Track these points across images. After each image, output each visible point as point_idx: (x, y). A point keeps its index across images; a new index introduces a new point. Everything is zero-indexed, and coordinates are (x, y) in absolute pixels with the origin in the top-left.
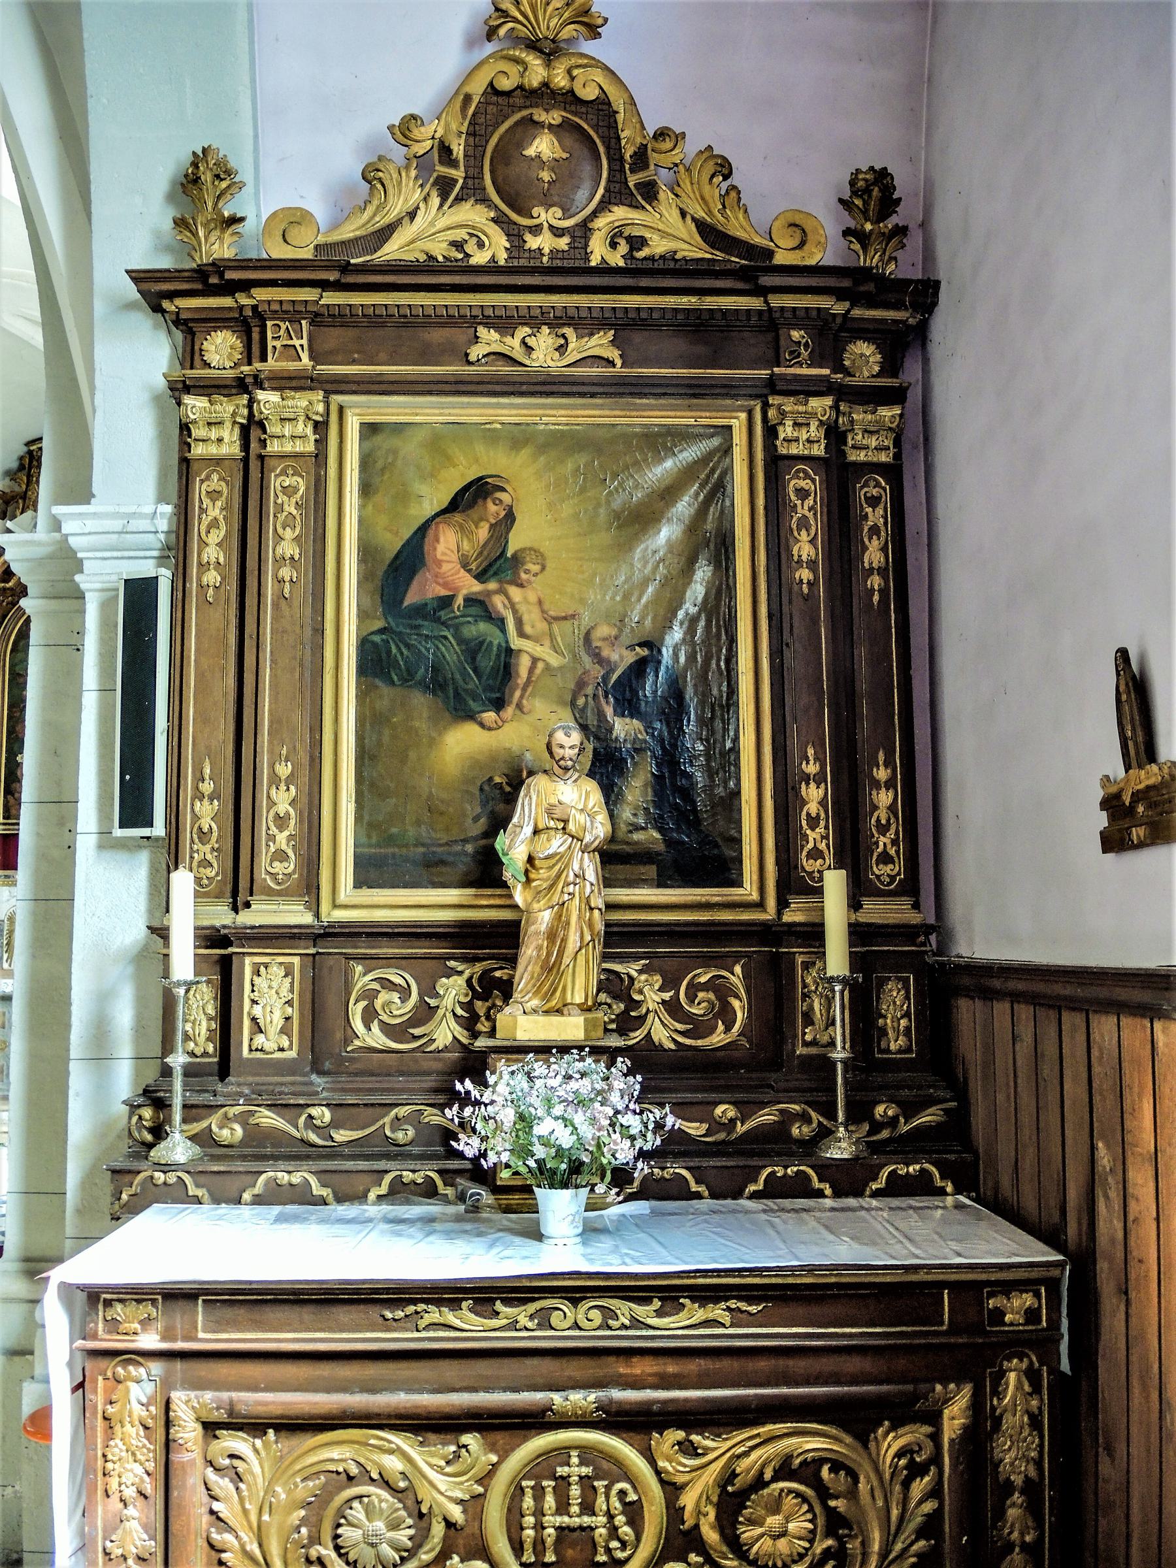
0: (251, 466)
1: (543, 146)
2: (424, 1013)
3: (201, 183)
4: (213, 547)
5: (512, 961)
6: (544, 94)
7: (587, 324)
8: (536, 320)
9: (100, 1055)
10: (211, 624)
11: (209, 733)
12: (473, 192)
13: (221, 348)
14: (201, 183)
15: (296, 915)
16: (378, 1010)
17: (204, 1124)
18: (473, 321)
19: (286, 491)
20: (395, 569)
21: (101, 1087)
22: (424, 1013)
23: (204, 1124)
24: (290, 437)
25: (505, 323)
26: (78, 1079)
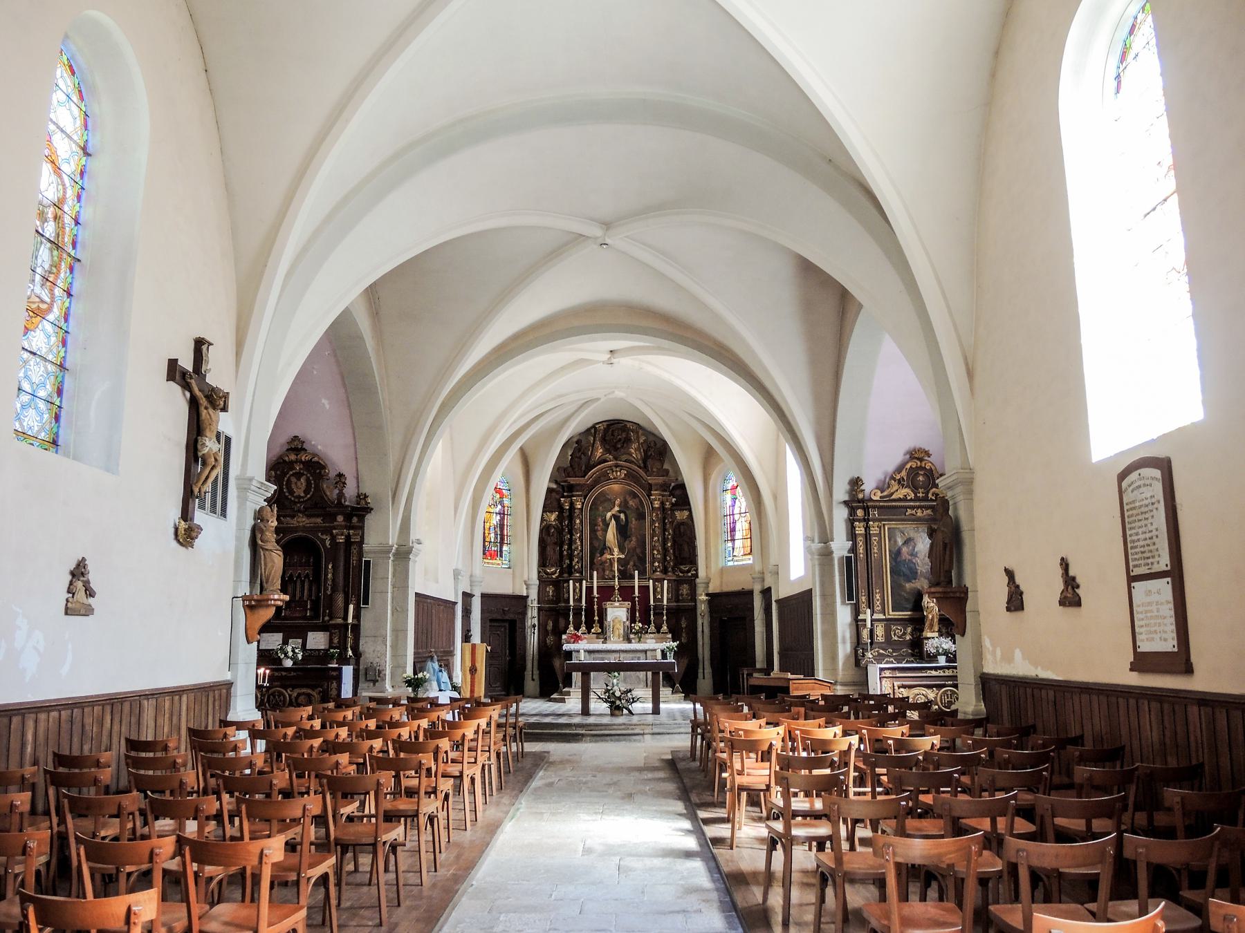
0: (867, 536)
1: (921, 478)
2: (904, 634)
3: (856, 483)
4: (861, 550)
5: (1005, 903)
6: (921, 468)
7: (927, 508)
8: (918, 507)
9: (844, 642)
10: (861, 567)
11: (862, 583)
12: (908, 486)
13: (860, 513)
14: (856, 483)
15: (881, 616)
16: (897, 631)
17: (783, 675)
18: (906, 507)
19: (875, 540)
20: (896, 554)
21: (845, 649)
22: (904, 634)
23: (783, 675)
24: (874, 531)
25: (912, 508)
26: (840, 646)
